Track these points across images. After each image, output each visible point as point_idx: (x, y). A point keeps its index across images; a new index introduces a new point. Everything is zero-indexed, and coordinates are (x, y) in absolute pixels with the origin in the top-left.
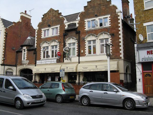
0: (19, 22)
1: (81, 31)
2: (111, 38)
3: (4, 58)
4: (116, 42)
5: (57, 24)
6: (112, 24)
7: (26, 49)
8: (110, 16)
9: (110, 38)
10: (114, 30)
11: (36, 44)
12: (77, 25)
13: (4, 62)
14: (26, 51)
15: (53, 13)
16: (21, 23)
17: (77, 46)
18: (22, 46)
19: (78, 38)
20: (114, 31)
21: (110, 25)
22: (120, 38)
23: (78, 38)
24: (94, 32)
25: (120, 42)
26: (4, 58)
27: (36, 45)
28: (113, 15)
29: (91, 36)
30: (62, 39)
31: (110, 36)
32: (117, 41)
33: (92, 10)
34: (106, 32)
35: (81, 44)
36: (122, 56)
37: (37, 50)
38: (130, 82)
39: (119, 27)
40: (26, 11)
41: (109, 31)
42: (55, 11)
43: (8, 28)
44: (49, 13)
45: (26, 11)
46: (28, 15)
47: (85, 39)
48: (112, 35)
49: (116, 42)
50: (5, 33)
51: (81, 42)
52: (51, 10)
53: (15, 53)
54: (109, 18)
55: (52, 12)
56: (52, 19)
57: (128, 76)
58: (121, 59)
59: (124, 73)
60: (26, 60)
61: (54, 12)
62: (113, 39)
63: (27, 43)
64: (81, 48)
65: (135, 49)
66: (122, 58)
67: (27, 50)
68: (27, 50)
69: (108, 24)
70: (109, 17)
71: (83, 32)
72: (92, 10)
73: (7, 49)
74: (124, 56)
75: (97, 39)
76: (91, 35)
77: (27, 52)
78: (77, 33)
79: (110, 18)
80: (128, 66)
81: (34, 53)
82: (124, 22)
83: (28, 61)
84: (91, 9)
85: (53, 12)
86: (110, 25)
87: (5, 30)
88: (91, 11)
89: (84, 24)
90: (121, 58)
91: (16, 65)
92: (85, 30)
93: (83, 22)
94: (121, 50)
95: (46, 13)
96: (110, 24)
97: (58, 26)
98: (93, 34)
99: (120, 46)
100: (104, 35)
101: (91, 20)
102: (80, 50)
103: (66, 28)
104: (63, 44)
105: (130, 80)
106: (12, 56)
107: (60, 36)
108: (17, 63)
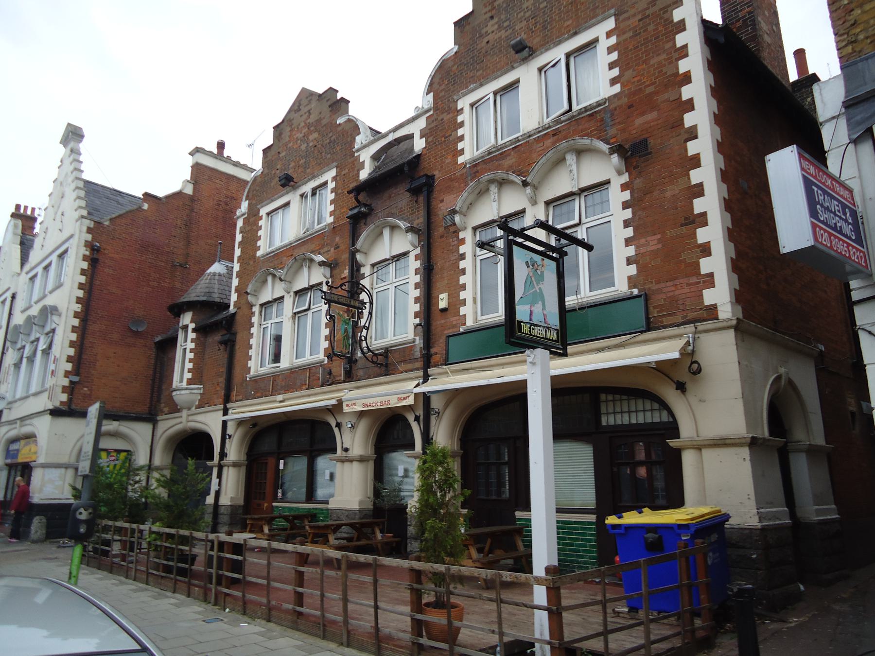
0: (178, 195)
1: (436, 173)
2: (625, 178)
3: (76, 379)
4: (668, 194)
5: (323, 167)
6: (629, 73)
7: (192, 326)
8: (610, 24)
9: (620, 173)
10: (643, 114)
11: (237, 291)
12: (419, 145)
13: (70, 400)
14: (192, 335)
15: (309, 111)
16: (192, 199)
17: (417, 272)
18: (178, 310)
19: (420, 221)
20: (649, 117)
21: (617, 88)
22: (696, 162)
23: (421, 220)
24: (507, 162)
25: (698, 191)
26: (76, 379)
27: (234, 297)
28: (632, 12)
29: (494, 189)
30: (342, 240)
31: (615, 158)
32: (671, 191)
33: (500, 28)
34: (586, 141)
35: (439, 262)
36: (720, 295)
37: (239, 326)
38: (763, 529)
39: (687, 78)
40: (221, 145)
41: (612, 131)
42: (320, 95)
43: (107, 223)
44: (293, 115)
45: (221, 145)
46: (237, 164)
47: (457, 218)
48: (633, 154)
49: (668, 194)
50: (89, 245)
51: (437, 243)
52: (306, 97)
53: (152, 353)
54: (605, 43)
55: (306, 110)
56: (303, 147)
57: (800, 465)
58: (709, 325)
59: (754, 443)
60: (189, 382)
61: (313, 105)
62: (638, 182)
63: (196, 293)
64: (440, 282)
65: (826, 133)
66: (726, 311)
67: (194, 330)
68: (194, 330)
69: (598, 82)
70: (609, 35)
71: (451, 179)
72: (500, 28)
73: (93, 327)
74: (739, 297)
75: (534, 203)
76: (491, 181)
77: (197, 338)
78: (415, 192)
79: (613, 40)
80: (790, 382)
81: (224, 343)
82: (722, 40)
83: (198, 389)
84: (492, 26)
85: (308, 108)
86: (617, 88)
87: (89, 230)
88: (493, 31)
89: (456, 130)
90: (712, 312)
91: (150, 413)
92: (461, 160)
93: (446, 117)
94: (705, 249)
95: (283, 121)
96: (613, 82)
97: (329, 175)
98: (500, 174)
99: (702, 220)
100: (574, 167)
101: (495, 93)
102: (434, 292)
103: (364, 175)
104: (346, 273)
105: (818, 500)
106: (122, 366)
107: (334, 229)
108: (159, 401)
